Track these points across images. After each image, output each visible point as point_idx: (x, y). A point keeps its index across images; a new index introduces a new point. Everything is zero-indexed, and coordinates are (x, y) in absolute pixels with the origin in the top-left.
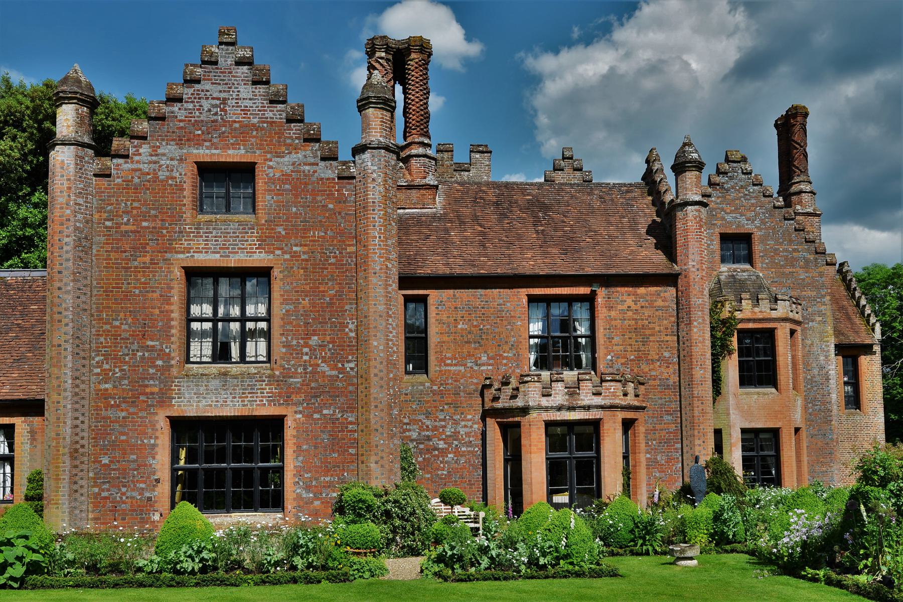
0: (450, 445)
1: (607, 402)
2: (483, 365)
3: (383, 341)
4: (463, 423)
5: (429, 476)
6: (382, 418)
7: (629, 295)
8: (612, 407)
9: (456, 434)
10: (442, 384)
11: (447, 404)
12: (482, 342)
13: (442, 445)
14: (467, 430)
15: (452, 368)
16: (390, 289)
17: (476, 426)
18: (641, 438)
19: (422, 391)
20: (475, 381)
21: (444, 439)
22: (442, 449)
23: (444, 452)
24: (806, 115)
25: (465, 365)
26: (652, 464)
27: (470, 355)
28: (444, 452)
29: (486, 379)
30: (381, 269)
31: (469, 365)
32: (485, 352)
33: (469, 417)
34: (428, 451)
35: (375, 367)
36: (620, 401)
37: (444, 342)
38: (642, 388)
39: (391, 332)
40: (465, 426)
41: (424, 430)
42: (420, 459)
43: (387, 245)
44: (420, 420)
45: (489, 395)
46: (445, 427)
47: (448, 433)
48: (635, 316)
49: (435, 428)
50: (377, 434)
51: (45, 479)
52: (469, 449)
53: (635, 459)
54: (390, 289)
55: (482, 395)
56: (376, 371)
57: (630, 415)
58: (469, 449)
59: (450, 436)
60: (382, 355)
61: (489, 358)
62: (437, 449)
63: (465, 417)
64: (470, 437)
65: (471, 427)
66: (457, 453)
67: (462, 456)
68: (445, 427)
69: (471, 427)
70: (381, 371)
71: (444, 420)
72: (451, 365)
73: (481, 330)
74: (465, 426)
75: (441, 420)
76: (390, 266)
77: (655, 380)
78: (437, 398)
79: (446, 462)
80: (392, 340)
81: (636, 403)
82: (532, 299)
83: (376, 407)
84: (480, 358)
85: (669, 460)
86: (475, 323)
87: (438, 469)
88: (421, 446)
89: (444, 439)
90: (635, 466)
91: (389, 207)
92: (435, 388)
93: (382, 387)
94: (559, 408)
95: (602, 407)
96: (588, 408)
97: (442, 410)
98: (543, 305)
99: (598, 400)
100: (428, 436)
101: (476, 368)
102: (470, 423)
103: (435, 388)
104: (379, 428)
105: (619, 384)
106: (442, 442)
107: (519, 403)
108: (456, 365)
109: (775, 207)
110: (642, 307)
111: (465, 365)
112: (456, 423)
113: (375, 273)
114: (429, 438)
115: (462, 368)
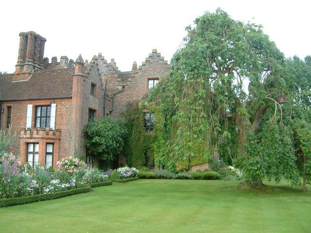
94: (28, 138)
99: (37, 136)
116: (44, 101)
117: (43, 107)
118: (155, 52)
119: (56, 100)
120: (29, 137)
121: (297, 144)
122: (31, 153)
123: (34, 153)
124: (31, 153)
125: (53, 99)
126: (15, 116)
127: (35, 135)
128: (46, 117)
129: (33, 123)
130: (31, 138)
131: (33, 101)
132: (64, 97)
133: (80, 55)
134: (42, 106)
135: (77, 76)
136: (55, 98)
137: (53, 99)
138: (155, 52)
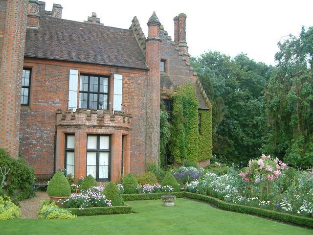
0: (38, 142)
1: (117, 125)
2: (57, 103)
3: (14, 86)
4: (45, 132)
5: (27, 157)
6: (11, 126)
7: (126, 76)
8: (119, 127)
9: (41, 138)
10: (36, 112)
11: (38, 122)
12: (57, 92)
13: (34, 142)
14: (47, 135)
15: (43, 104)
16: (20, 58)
17: (52, 134)
18: (129, 144)
19: (26, 114)
20: (52, 111)
21: (35, 139)
22: (34, 144)
23: (35, 145)
24: (186, 17)
25: (48, 103)
26: (133, 155)
27: (51, 98)
28: (35, 145)
29: (58, 110)
30: (16, 47)
31: (50, 103)
32: (58, 97)
33: (49, 129)
34: (28, 144)
35: (9, 98)
36: (123, 125)
37: (39, 91)
38: (130, 120)
39: (19, 81)
40: (46, 133)
41: (25, 134)
42: (23, 149)
43: (21, 36)
44: (24, 129)
45: (60, 117)
46: (36, 133)
47: (38, 136)
48: (128, 87)
49: (31, 133)
50: (8, 134)
51: (159, 90)
52: (48, 145)
53: (126, 153)
54: (20, 58)
55: (56, 117)
56: (9, 100)
57: (125, 132)
58: (48, 145)
59: (39, 138)
60: (13, 92)
61: (60, 100)
62: (32, 144)
63: (47, 129)
64: (48, 139)
65: (49, 134)
66: (41, 146)
67: (44, 148)
68: (36, 133)
69: (49, 134)
70: (12, 101)
71: (36, 129)
72: (41, 102)
73: (57, 86)
74: (46, 133)
75: (34, 130)
76: (21, 46)
77: (136, 116)
78: (33, 118)
79: (36, 151)
80: (18, 85)
81: (128, 126)
82: (82, 74)
83: (8, 119)
84: (55, 100)
85: (140, 154)
86: (54, 82)
87: (32, 154)
88: (24, 142)
89: (35, 139)
90: (126, 156)
91: (24, 17)
92: (32, 113)
93: (12, 109)
94: (95, 127)
95: (114, 127)
96: (109, 127)
97: (35, 125)
98: (86, 78)
99: (112, 124)
100: (28, 137)
101: (53, 105)
102: (49, 132)
103: (32, 113)
104: (9, 131)
105: (122, 117)
106: (34, 141)
107: (74, 123)
108: (43, 102)
109: (175, 50)
110: (132, 83)
111: (48, 103)
112: (42, 131)
113: (13, 49)
114: (28, 138)
115: (46, 104)
116: (99, 68)
117: (92, 78)
118: (94, 16)
119: (120, 70)
120: (95, 123)
121: (80, 125)
122: (104, 151)
123: (98, 151)
124: (104, 151)
125: (118, 67)
126: (41, 87)
127: (107, 122)
128: (108, 94)
129: (110, 103)
130: (100, 127)
131: (79, 66)
132: (137, 67)
133: (154, 14)
134: (99, 76)
135: (158, 42)
136: (120, 67)
137: (118, 68)
138: (94, 16)
